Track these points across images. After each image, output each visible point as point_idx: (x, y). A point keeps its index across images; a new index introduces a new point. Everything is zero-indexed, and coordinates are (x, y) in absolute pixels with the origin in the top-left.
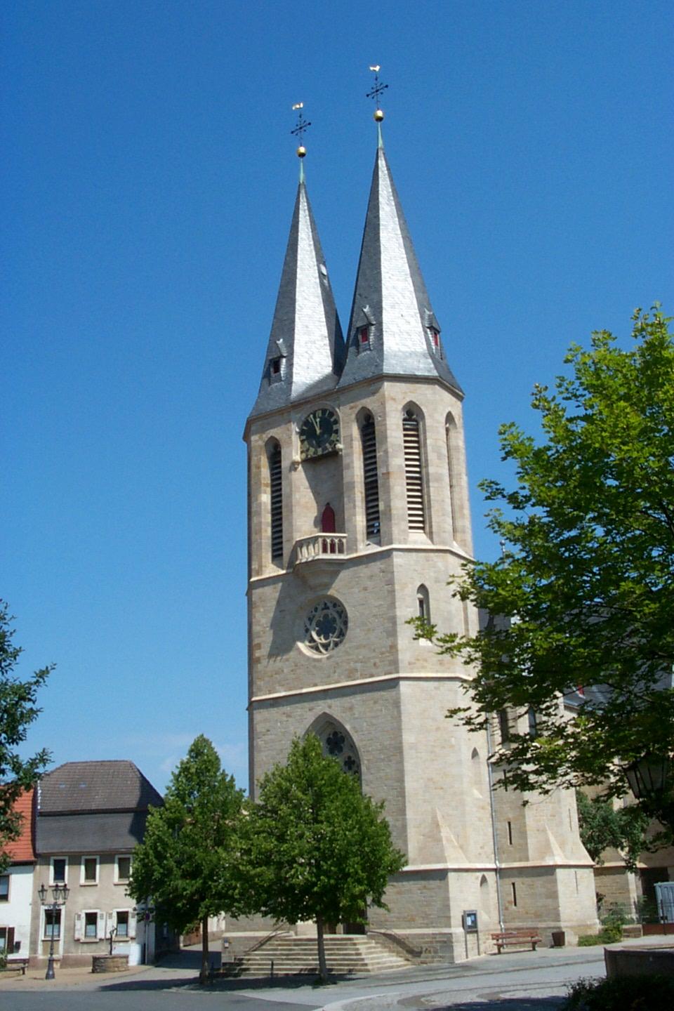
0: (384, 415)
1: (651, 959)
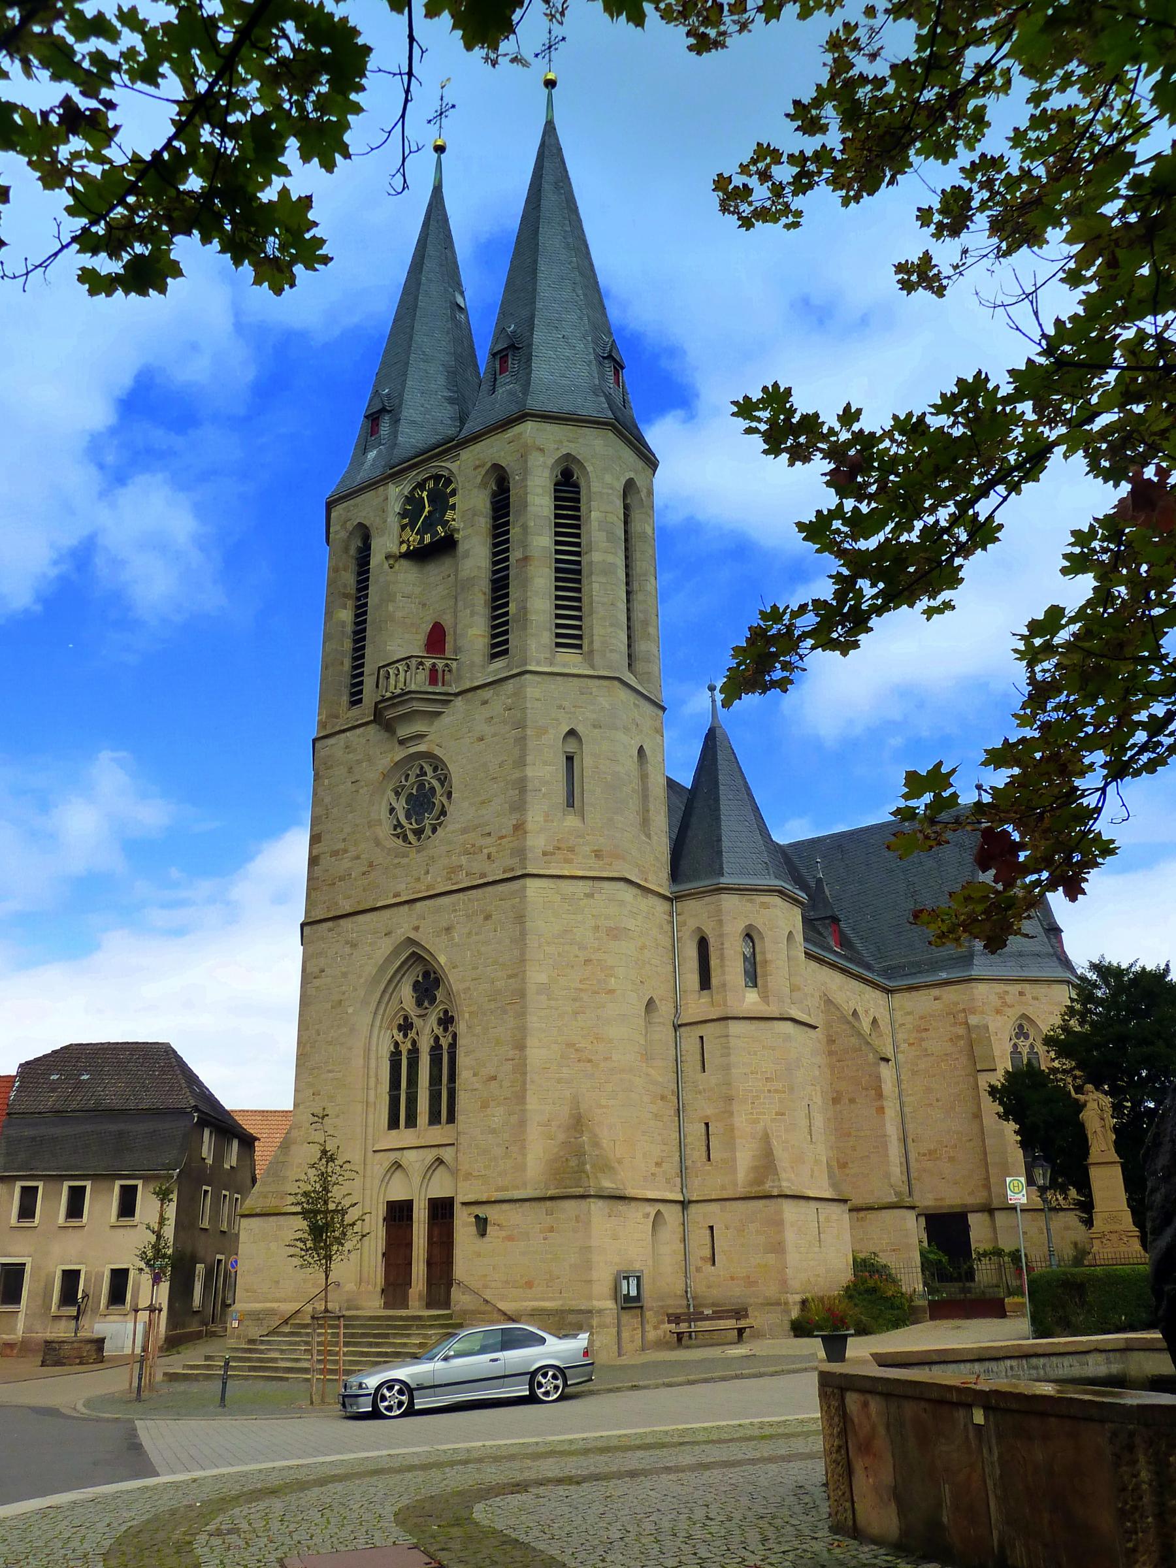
0: (525, 472)
1: (979, 1417)
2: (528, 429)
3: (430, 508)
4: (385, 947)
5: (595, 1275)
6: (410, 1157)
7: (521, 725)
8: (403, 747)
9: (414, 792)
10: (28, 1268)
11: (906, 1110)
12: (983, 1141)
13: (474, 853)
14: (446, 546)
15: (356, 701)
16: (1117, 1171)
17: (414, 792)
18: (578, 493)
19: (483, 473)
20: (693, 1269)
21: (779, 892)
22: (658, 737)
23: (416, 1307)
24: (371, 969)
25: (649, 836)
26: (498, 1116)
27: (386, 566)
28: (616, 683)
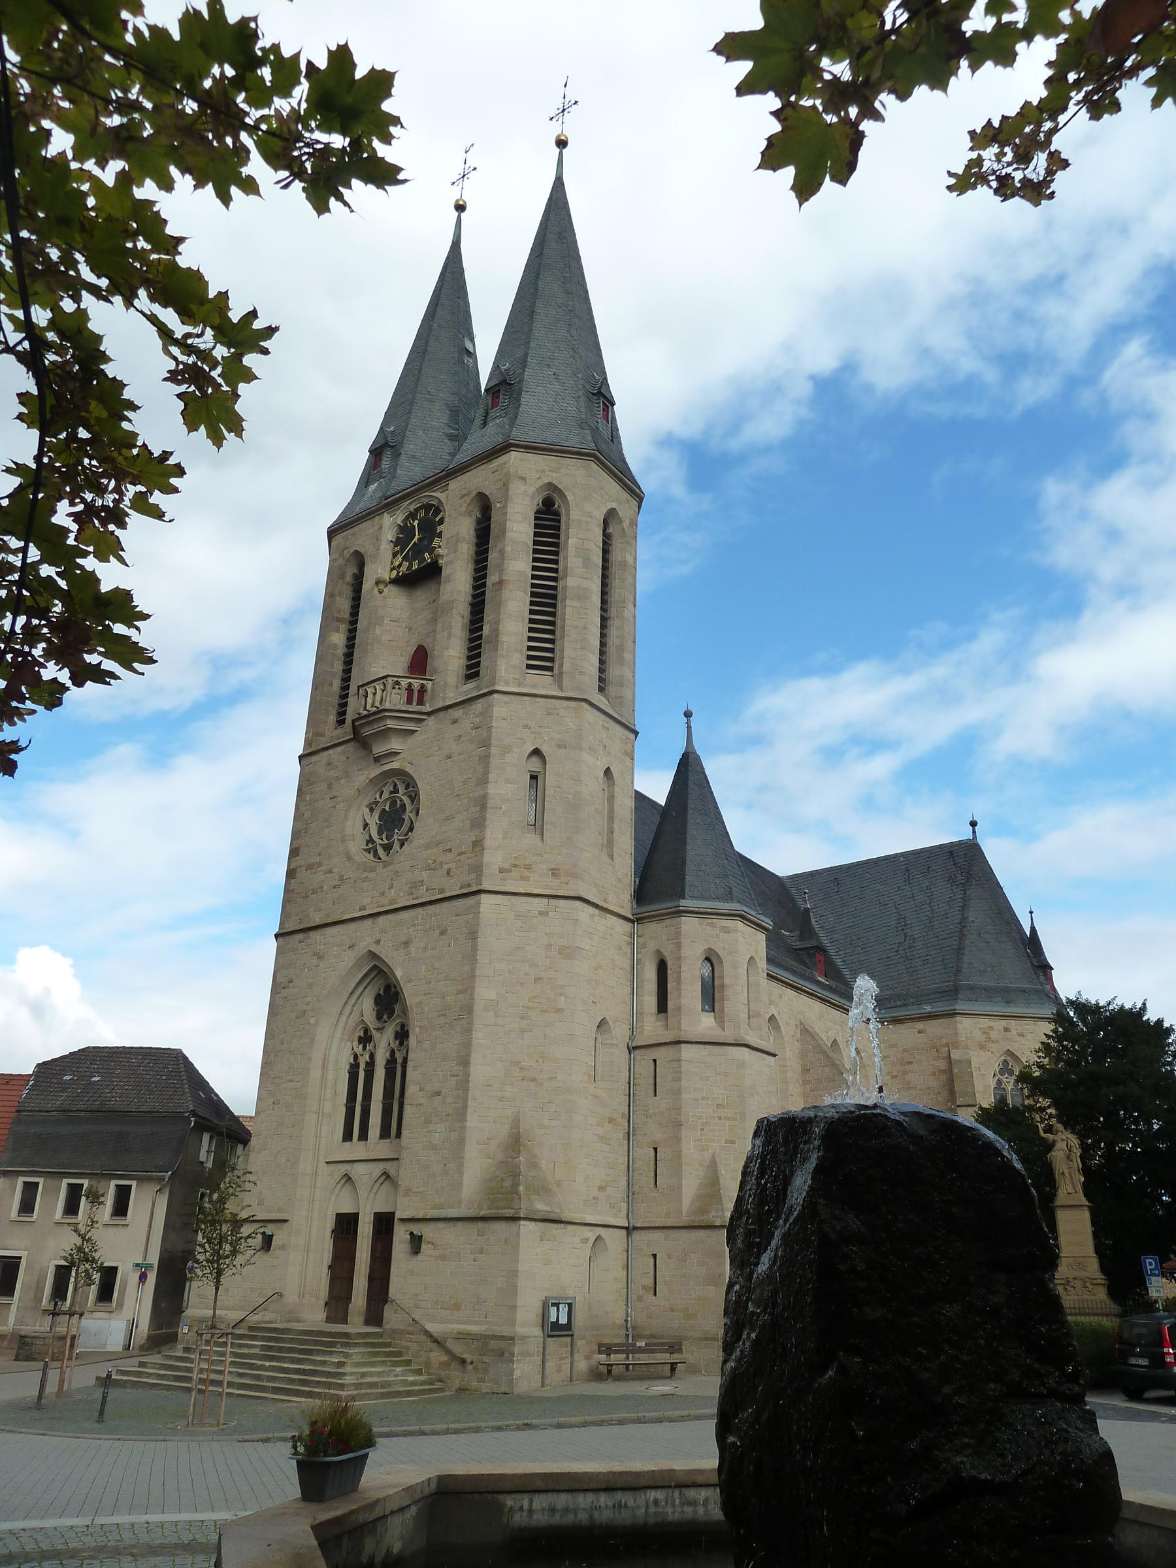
0: (506, 499)
4: (348, 959)
5: (520, 1301)
6: (358, 1171)
7: (486, 744)
9: (387, 808)
10: (23, 1262)
13: (435, 869)
15: (341, 722)
16: (1086, 1215)
17: (387, 808)
18: (559, 521)
21: (741, 916)
22: (628, 760)
23: (356, 1325)
25: (611, 857)
26: (439, 1131)
27: (376, 590)
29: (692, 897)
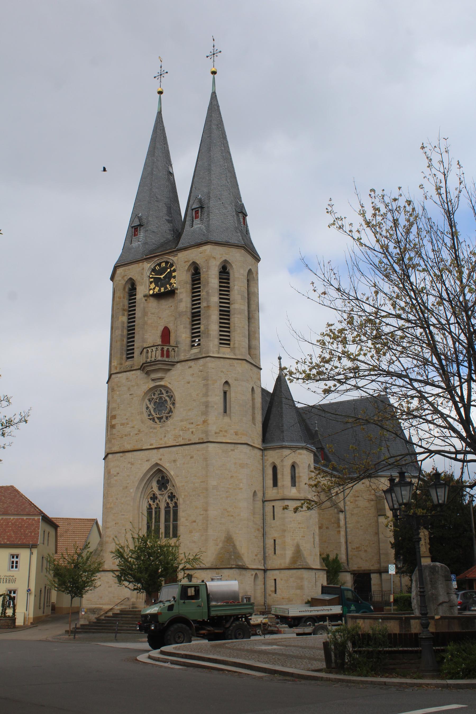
0: (208, 268)
2: (208, 248)
3: (162, 276)
4: (147, 466)
7: (206, 379)
8: (153, 382)
9: (157, 401)
11: (348, 530)
12: (379, 544)
13: (186, 431)
14: (171, 293)
18: (229, 276)
19: (189, 264)
20: (267, 595)
21: (306, 448)
24: (141, 475)
25: (255, 424)
28: (244, 361)
29: (287, 441)
